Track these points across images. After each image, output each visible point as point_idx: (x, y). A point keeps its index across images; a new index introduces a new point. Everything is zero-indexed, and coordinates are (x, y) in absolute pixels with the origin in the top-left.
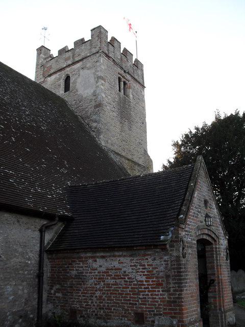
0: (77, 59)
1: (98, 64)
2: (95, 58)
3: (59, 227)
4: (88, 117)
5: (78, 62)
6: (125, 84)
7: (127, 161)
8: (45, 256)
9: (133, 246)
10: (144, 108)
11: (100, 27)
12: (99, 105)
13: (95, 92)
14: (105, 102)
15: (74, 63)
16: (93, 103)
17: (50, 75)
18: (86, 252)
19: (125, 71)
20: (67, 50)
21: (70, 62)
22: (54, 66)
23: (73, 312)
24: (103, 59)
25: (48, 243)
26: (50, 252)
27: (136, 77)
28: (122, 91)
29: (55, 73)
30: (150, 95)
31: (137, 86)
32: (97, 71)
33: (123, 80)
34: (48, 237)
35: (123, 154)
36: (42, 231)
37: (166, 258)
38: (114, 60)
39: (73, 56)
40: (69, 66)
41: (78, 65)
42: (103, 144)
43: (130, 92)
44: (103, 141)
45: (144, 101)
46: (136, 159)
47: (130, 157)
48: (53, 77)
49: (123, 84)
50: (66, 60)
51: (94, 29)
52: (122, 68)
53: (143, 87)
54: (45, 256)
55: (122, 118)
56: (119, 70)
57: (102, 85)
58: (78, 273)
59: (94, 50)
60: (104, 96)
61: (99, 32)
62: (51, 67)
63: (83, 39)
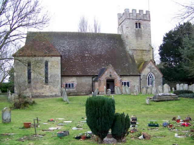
28: (138, 27)
33: (138, 23)
35: (138, 49)
43: (142, 26)
46: (144, 49)
47: (141, 49)
49: (138, 25)
52: (136, 19)
56: (136, 21)
60: (128, 33)
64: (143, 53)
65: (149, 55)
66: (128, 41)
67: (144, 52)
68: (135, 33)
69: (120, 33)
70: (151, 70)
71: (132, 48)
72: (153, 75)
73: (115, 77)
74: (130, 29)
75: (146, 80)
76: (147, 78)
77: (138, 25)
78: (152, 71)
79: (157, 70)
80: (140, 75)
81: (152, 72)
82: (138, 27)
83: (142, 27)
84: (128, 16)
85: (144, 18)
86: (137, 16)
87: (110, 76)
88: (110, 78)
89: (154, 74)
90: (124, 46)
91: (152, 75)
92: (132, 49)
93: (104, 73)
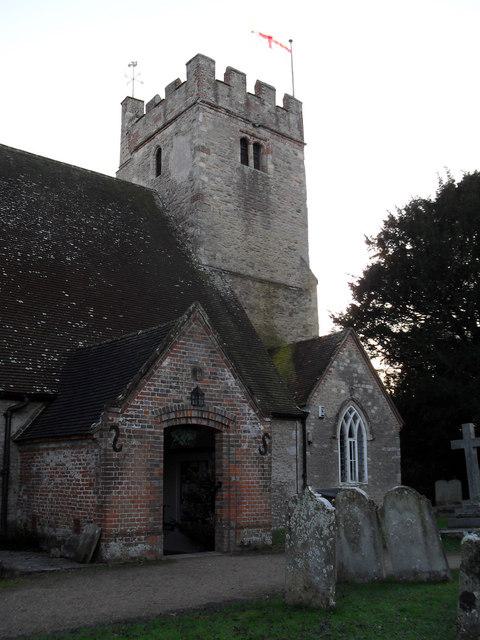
0: (169, 118)
1: (195, 125)
2: (191, 114)
3: (35, 410)
4: (183, 219)
5: (170, 123)
6: (257, 146)
7: (258, 285)
8: (14, 449)
9: (70, 436)
10: (302, 183)
11: (198, 57)
12: (198, 197)
13: (191, 173)
14: (208, 190)
15: (165, 126)
16: (190, 194)
17: (137, 149)
18: (49, 442)
19: (254, 125)
20: (157, 102)
21: (160, 124)
22: (141, 132)
23: (34, 519)
24: (203, 116)
25: (18, 433)
26: (19, 442)
27: (284, 130)
28: (251, 161)
29: (142, 144)
30: (314, 158)
31: (286, 147)
32: (193, 137)
33: (252, 140)
34: (17, 424)
35: (251, 272)
36: (9, 415)
37: (96, 450)
38: (228, 111)
39: (165, 113)
40: (159, 131)
41: (171, 129)
42: (204, 261)
43: (269, 161)
44: (203, 258)
45: (302, 171)
46: (279, 278)
47: (266, 276)
48: (141, 151)
49: (251, 151)
50: (156, 120)
51: (190, 61)
52: (247, 121)
53: (301, 144)
54: (14, 449)
55: (247, 210)
56: (242, 125)
57: (202, 160)
58: (151, 465)
59: (191, 100)
60: (206, 179)
61: (199, 66)
62: (137, 135)
63: (178, 80)
64: (276, 302)
65: (301, 314)
66: (205, 221)
67: (281, 292)
68: (241, 186)
69: (143, 180)
70: (352, 391)
71: (224, 260)
72: (361, 419)
73: (230, 414)
74: (213, 157)
75: (331, 449)
76: (334, 438)
77: (251, 151)
78: (356, 396)
79: (376, 394)
80: (302, 418)
81: (357, 402)
82: (251, 161)
83: (271, 167)
84: (210, 93)
85: (277, 124)
86: (248, 104)
87: (197, 395)
88: (194, 417)
89: (367, 417)
90: (177, 244)
91: (355, 418)
92: (225, 266)
93: (147, 374)
